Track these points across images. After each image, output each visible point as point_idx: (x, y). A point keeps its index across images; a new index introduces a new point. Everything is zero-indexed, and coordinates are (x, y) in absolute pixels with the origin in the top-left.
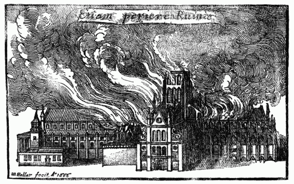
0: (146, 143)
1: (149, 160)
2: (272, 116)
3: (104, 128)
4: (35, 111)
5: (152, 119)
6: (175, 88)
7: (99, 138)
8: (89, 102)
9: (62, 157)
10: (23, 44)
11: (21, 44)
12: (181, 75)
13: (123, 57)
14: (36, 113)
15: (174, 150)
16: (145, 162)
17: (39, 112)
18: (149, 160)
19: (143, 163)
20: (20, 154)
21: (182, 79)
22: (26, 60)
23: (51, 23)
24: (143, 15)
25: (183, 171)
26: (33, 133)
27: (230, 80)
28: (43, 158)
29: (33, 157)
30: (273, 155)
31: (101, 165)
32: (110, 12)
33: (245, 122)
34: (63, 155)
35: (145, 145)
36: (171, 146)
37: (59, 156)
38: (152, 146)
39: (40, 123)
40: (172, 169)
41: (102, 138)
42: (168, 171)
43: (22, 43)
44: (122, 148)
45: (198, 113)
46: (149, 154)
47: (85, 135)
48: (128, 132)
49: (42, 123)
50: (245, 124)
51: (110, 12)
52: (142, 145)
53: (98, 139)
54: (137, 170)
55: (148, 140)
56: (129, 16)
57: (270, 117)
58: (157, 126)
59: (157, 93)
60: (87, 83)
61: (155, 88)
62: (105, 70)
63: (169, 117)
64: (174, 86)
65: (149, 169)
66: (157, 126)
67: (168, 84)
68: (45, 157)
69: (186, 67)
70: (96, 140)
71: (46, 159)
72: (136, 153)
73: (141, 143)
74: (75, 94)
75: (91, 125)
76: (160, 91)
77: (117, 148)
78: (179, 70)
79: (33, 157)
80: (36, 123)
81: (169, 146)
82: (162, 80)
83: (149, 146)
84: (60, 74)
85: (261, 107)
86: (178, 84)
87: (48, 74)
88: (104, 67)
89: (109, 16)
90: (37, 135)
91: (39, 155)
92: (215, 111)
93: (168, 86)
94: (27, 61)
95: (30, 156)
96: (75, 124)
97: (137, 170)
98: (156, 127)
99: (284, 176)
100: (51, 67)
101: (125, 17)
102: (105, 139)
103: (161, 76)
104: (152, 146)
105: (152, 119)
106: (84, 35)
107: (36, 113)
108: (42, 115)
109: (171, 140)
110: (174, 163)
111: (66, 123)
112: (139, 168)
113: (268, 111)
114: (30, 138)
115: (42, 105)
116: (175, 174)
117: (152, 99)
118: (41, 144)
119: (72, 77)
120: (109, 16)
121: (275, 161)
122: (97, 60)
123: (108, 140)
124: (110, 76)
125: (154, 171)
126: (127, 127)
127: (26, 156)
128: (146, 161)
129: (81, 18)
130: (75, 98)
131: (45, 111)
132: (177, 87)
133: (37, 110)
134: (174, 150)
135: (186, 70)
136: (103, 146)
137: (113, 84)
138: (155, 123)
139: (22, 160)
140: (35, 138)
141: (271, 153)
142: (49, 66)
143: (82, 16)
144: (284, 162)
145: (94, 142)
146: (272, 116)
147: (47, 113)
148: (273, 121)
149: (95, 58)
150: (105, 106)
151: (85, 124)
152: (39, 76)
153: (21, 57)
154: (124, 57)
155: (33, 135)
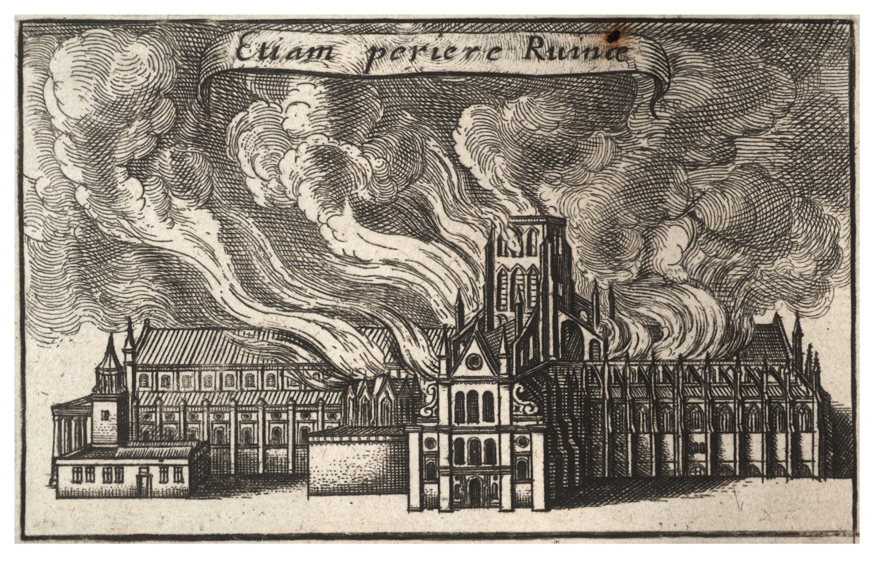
0: (438, 429)
1: (445, 481)
2: (810, 346)
3: (311, 385)
4: (107, 335)
5: (453, 360)
6: (522, 267)
7: (298, 415)
8: (265, 309)
9: (186, 471)
10: (70, 136)
11: (64, 138)
12: (539, 227)
13: (365, 175)
14: (111, 340)
15: (518, 449)
16: (434, 487)
17: (120, 341)
18: (445, 481)
19: (427, 487)
20: (58, 462)
21: (540, 241)
22: (81, 184)
23: (154, 74)
24: (424, 49)
25: (547, 509)
26: (105, 399)
27: (684, 241)
28: (130, 475)
29: (99, 471)
30: (813, 461)
31: (305, 490)
32: (323, 40)
33: (730, 367)
34: (190, 465)
35: (434, 436)
36: (512, 438)
37: (178, 469)
38: (454, 437)
39: (121, 372)
40: (517, 503)
41: (306, 414)
42: (440, 511)
43: (67, 134)
44: (365, 442)
45: (592, 342)
46: (443, 462)
47: (287, 405)
48: (383, 395)
49: (129, 369)
50: (730, 373)
51: (323, 40)
52: (426, 436)
53: (323, 417)
54: (410, 509)
55: (444, 420)
56: (383, 51)
57: (805, 349)
58: (469, 380)
59: (466, 280)
60: (261, 253)
61: (461, 268)
62: (312, 215)
63: (503, 351)
64: (517, 260)
65: (444, 504)
66: (469, 380)
67: (499, 255)
68: (135, 470)
69: (553, 202)
70: (288, 421)
71: (139, 478)
72: (288, 453)
73: (423, 428)
74: (226, 286)
75: (273, 376)
76: (476, 272)
77: (350, 442)
78: (531, 211)
79: (99, 471)
80: (109, 370)
81: (506, 437)
82: (483, 242)
83: (444, 439)
84: (178, 226)
85: (777, 318)
86: (529, 254)
87: (144, 226)
88: (310, 206)
89: (325, 52)
90: (112, 408)
91: (117, 466)
92: (637, 330)
93: (499, 261)
94: (82, 189)
95: (91, 469)
96: (225, 373)
97: (410, 509)
98: (466, 382)
99: (28, 533)
100: (153, 206)
101: (373, 54)
102: (314, 416)
103: (479, 233)
104: (454, 437)
105: (453, 360)
106: (250, 110)
107: (111, 340)
108: (129, 347)
109: (512, 418)
110: (427, 487)
111: (241, 371)
112: (415, 502)
113: (798, 334)
114: (91, 414)
115: (129, 319)
116: (522, 521)
117: (452, 300)
118: (123, 437)
119: (215, 237)
120: (325, 52)
121: (819, 479)
122: (288, 183)
123: (323, 422)
124: (326, 233)
125: (464, 512)
126: (379, 382)
127: (77, 470)
128: (438, 482)
129: (242, 59)
130: (220, 291)
131: (137, 334)
132: (526, 262)
133: (112, 333)
134: (518, 449)
135: (552, 212)
136: (306, 439)
137: (337, 256)
138: (462, 370)
139: (65, 475)
140: (106, 415)
141: (807, 455)
142: (148, 203)
143: (245, 52)
144: (849, 482)
145: (281, 426)
146: (810, 346)
147: (143, 340)
148: (814, 362)
149: (285, 179)
150: (233, 310)
151: (255, 373)
152: (117, 233)
153: (65, 177)
154: (369, 174)
155: (99, 407)
